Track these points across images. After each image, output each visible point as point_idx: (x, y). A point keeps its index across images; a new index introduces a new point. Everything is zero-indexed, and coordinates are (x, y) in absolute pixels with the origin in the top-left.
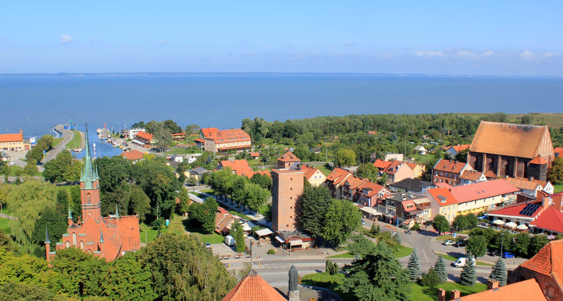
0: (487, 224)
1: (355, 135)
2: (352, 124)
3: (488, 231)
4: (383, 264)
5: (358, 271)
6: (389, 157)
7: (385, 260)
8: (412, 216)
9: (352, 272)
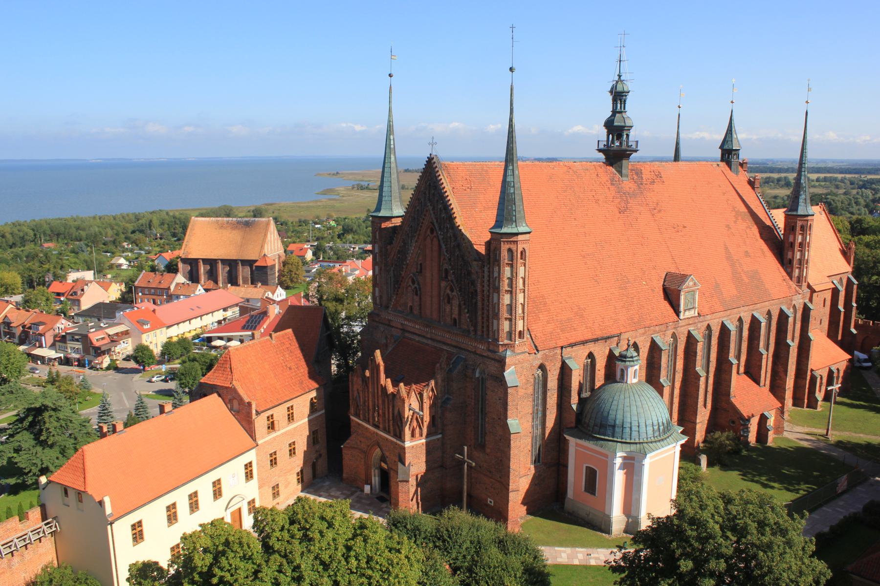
0: (205, 348)
1: (22, 251)
2: (17, 235)
3: (203, 356)
4: (50, 416)
5: (18, 433)
6: (72, 276)
7: (55, 410)
8: (105, 351)
9: (11, 436)
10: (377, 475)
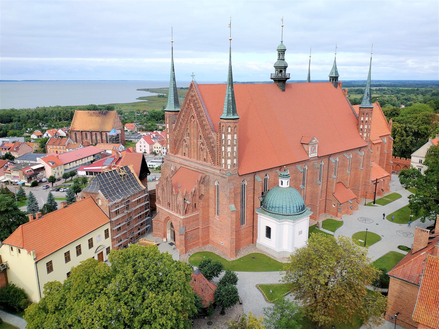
10: (169, 232)
